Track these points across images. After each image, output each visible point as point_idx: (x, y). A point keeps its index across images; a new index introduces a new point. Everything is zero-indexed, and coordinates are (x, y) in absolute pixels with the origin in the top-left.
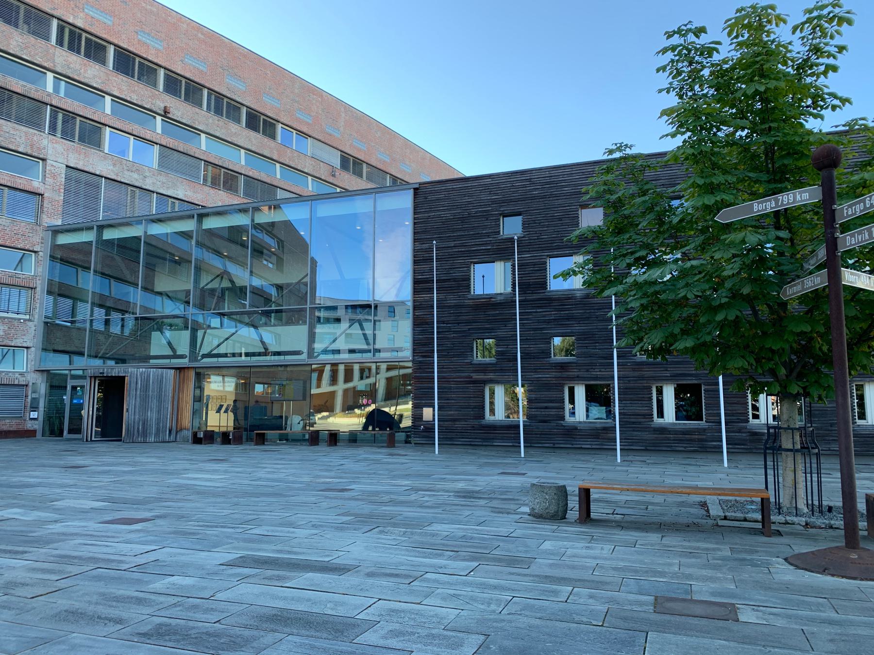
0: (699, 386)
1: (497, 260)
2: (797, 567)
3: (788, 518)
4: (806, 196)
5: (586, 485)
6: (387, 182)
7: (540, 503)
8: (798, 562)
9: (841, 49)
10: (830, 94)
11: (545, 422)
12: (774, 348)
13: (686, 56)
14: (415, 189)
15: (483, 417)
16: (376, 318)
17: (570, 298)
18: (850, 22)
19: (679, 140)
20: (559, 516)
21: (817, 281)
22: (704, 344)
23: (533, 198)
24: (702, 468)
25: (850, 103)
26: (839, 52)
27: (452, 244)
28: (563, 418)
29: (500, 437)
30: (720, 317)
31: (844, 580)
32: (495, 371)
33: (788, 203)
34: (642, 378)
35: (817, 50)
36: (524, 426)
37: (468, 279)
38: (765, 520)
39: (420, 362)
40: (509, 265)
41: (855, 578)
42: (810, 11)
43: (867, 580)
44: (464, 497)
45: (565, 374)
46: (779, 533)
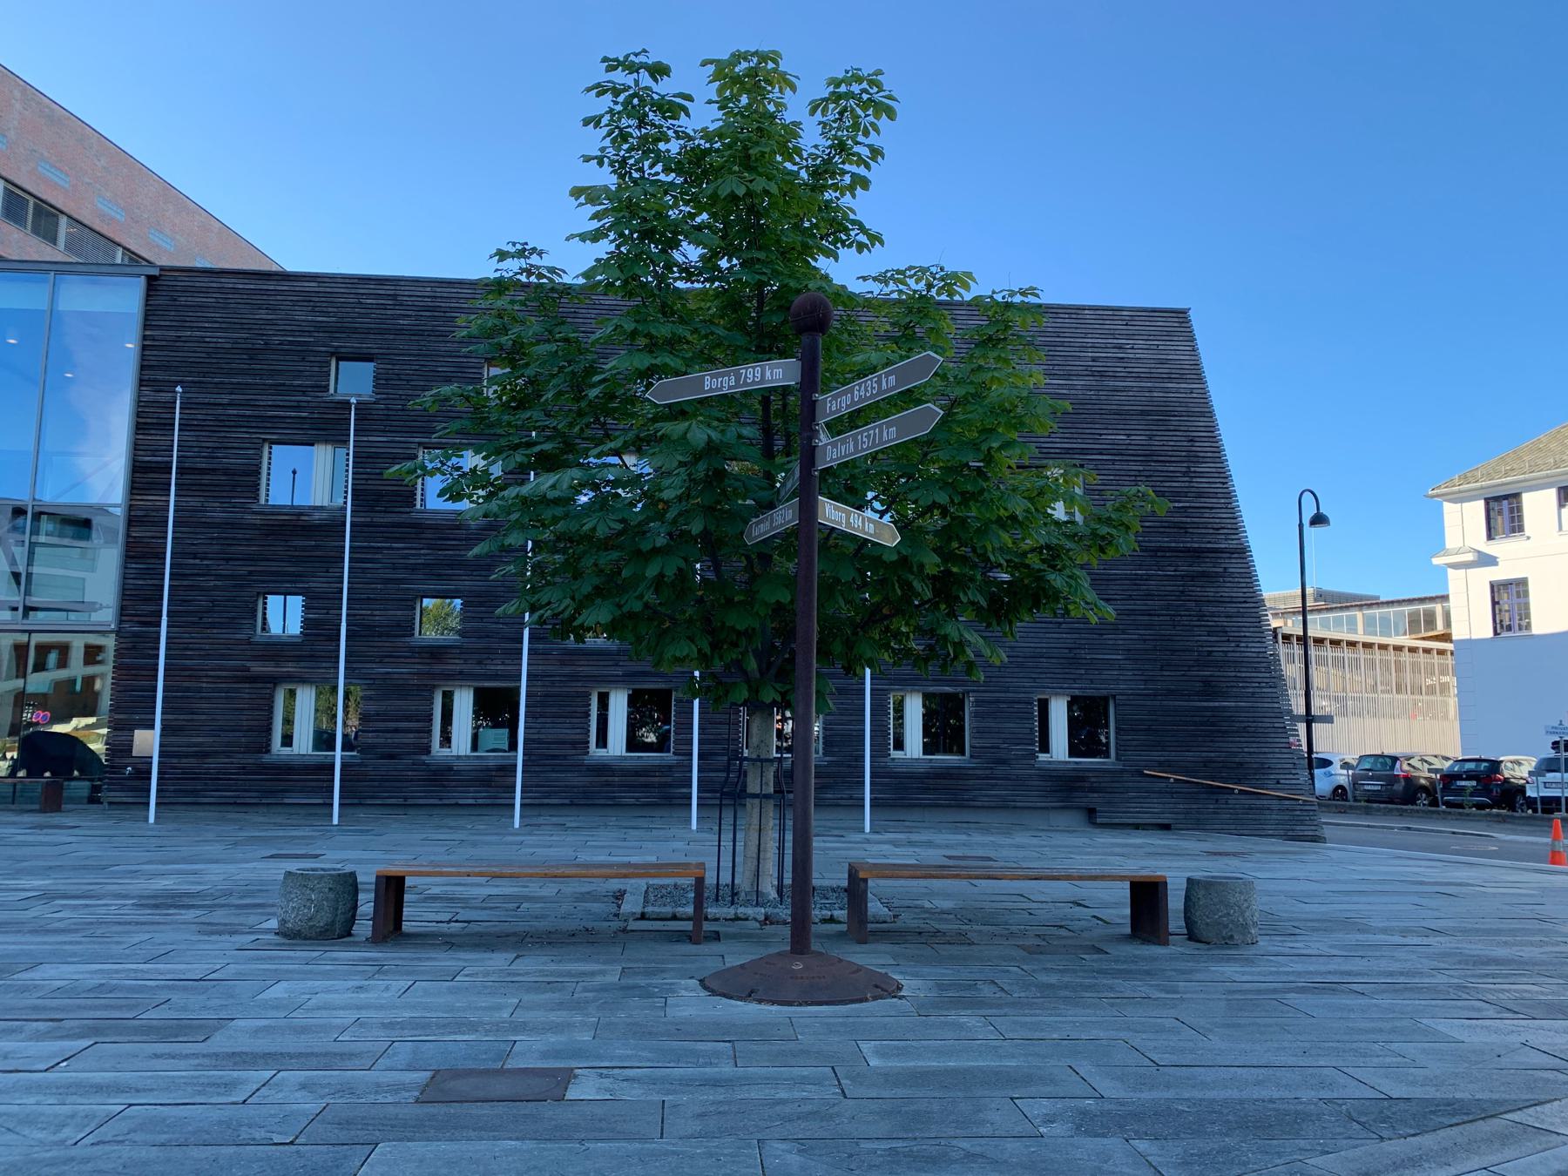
0: (668, 693)
1: (319, 442)
2: (714, 993)
3: (741, 910)
4: (779, 372)
5: (394, 870)
6: (98, 255)
7: (313, 908)
8: (719, 986)
9: (876, 152)
10: (854, 222)
11: (391, 757)
12: (738, 627)
13: (637, 111)
14: (151, 279)
15: (267, 748)
16: (34, 539)
17: (458, 527)
18: (891, 114)
19: (604, 248)
20: (338, 931)
21: (785, 516)
22: (631, 615)
23: (400, 332)
24: (655, 832)
25: (882, 243)
26: (874, 159)
27: (225, 399)
28: (427, 750)
29: (289, 788)
30: (652, 571)
31: (775, 1008)
32: (299, 659)
33: (754, 383)
34: (574, 677)
35: (841, 147)
36: (343, 765)
37: (257, 473)
38: (699, 916)
39: (135, 635)
40: (341, 452)
41: (790, 1004)
42: (837, 83)
43: (812, 1004)
44: (156, 906)
45: (438, 668)
46: (716, 937)
